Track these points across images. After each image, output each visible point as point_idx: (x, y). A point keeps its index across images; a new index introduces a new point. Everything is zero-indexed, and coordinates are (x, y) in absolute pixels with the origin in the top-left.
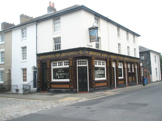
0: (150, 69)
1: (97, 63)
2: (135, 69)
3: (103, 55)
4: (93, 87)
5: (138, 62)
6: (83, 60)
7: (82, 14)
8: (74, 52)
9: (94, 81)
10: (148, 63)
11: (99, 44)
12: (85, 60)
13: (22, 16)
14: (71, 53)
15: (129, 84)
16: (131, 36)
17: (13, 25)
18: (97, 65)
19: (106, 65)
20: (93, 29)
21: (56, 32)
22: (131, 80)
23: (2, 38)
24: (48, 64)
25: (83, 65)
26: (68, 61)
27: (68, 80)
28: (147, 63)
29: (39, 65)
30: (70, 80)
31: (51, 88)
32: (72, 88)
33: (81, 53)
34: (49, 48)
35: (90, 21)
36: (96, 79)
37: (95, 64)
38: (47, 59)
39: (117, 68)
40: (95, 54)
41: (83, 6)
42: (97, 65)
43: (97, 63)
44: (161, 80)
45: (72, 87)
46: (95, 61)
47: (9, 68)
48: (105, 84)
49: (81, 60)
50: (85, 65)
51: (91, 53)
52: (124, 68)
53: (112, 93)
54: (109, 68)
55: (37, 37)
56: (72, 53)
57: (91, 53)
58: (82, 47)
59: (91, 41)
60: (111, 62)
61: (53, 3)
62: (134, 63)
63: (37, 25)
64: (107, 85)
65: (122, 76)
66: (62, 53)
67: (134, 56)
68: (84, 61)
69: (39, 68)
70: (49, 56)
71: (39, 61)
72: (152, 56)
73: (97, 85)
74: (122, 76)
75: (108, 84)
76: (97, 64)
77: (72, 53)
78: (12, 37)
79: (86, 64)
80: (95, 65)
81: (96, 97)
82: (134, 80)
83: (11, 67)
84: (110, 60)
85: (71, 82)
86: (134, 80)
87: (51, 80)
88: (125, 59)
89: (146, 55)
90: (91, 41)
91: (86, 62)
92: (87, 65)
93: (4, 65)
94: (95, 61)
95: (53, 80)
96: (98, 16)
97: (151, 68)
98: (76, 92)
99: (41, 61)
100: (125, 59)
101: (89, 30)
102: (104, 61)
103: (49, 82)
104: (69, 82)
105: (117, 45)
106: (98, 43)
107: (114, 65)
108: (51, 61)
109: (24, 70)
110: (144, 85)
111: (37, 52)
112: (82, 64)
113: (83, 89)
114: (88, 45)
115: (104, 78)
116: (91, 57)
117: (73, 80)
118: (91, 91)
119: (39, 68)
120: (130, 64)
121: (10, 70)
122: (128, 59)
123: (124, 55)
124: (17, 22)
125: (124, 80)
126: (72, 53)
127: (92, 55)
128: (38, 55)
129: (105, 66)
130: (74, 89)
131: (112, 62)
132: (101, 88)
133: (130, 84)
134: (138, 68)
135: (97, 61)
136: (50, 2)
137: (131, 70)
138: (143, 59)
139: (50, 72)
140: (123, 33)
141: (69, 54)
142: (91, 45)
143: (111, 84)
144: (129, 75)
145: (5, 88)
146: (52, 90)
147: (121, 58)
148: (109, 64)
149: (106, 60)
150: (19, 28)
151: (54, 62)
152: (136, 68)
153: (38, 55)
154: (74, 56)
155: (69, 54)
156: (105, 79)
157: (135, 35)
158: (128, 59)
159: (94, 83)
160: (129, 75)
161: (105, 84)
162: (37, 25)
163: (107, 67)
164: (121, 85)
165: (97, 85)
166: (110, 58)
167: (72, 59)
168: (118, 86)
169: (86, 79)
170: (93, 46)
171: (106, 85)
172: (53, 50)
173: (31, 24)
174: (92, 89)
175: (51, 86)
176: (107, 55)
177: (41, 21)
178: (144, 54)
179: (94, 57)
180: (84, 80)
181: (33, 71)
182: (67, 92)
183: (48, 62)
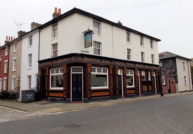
0: (176, 77)
1: (129, 72)
2: (152, 77)
4: (87, 96)
6: (78, 67)
7: (76, 17)
8: (67, 59)
9: (90, 90)
10: (173, 71)
12: (80, 67)
13: (33, 24)
14: (65, 60)
15: (143, 93)
16: (147, 41)
17: (24, 32)
18: (128, 74)
19: (134, 74)
20: (88, 33)
21: (55, 38)
22: (146, 90)
23: (16, 46)
24: (47, 71)
25: (78, 73)
26: (63, 68)
28: (173, 70)
29: (40, 72)
30: (64, 88)
31: (91, 97)
32: (65, 98)
33: (73, 59)
34: (47, 55)
35: (89, 24)
38: (47, 66)
39: (124, 76)
41: (75, 9)
42: (128, 74)
43: (129, 72)
44: (192, 89)
45: (65, 96)
46: (127, 71)
47: (19, 76)
48: (107, 93)
49: (76, 67)
50: (80, 73)
51: (86, 59)
52: (135, 76)
53: (101, 104)
54: (113, 75)
55: (39, 44)
56: (65, 59)
57: (86, 59)
58: (74, 53)
59: (86, 47)
60: (115, 69)
61: (60, 9)
62: (150, 71)
63: (40, 32)
66: (127, 62)
67: (151, 63)
68: (79, 68)
69: (40, 75)
70: (48, 63)
71: (40, 68)
72: (179, 63)
73: (94, 94)
75: (110, 93)
76: (128, 73)
77: (65, 59)
78: (22, 44)
79: (81, 71)
80: (127, 74)
81: (6, 106)
82: (150, 89)
83: (20, 74)
84: (115, 67)
85: (64, 90)
86: (150, 89)
89: (172, 61)
90: (86, 47)
91: (81, 69)
92: (82, 73)
93: (15, 73)
95: (51, 88)
96: (98, 20)
97: (177, 76)
98: (69, 102)
99: (42, 69)
100: (137, 65)
101: (85, 34)
102: (132, 71)
103: (47, 90)
104: (63, 91)
105: (126, 52)
106: (129, 54)
107: (120, 73)
108: (50, 68)
109: (30, 77)
110: (162, 95)
111: (39, 59)
112: (77, 71)
113: (77, 98)
114: (82, 51)
117: (66, 89)
118: (85, 101)
119: (40, 75)
121: (19, 77)
122: (141, 66)
123: (149, 63)
124: (28, 29)
125: (136, 89)
126: (66, 60)
128: (40, 62)
129: (107, 74)
130: (67, 98)
131: (118, 69)
132: (100, 98)
134: (157, 75)
135: (129, 71)
136: (56, 9)
137: (147, 78)
138: (161, 66)
139: (49, 79)
140: (135, 38)
141: (107, 62)
142: (87, 51)
143: (115, 93)
144: (143, 83)
145: (9, 95)
146: (49, 99)
147: (132, 65)
148: (113, 71)
149: (108, 67)
150: (27, 36)
151: (52, 70)
152: (154, 76)
153: (40, 62)
154: (67, 63)
155: (107, 62)
157: (152, 39)
158: (141, 66)
159: (89, 92)
160: (143, 83)
161: (107, 93)
162: (40, 32)
165: (94, 94)
166: (114, 65)
167: (66, 66)
168: (126, 96)
169: (81, 88)
170: (91, 51)
172: (52, 56)
174: (87, 99)
175: (48, 94)
176: (109, 62)
177: (44, 27)
178: (170, 60)
179: (91, 64)
180: (75, 89)
181: (36, 79)
182: (60, 101)
183: (47, 69)
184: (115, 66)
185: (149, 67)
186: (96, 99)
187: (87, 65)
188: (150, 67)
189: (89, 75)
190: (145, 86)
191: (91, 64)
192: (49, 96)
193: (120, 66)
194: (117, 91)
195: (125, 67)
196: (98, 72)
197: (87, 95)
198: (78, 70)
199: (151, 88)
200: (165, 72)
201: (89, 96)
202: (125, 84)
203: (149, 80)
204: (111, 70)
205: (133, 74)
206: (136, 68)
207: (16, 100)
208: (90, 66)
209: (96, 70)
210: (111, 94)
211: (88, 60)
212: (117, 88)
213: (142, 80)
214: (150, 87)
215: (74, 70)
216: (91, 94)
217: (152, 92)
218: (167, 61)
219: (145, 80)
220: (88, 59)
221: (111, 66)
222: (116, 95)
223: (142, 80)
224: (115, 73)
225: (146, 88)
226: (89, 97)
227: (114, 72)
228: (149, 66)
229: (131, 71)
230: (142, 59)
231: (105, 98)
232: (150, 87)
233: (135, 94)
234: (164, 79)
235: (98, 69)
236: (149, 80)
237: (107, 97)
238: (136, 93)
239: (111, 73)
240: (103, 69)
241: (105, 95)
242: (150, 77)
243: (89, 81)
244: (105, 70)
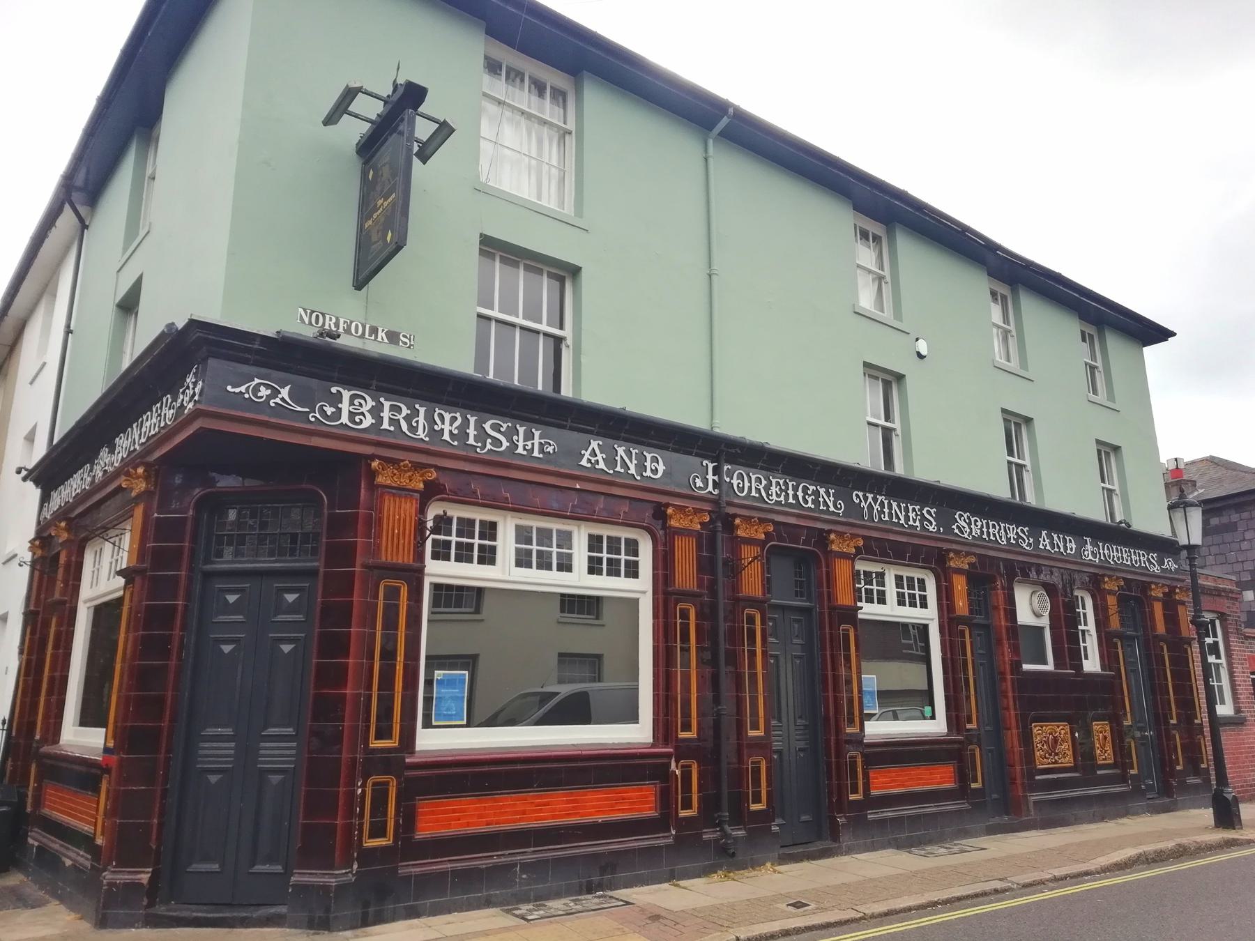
3: (1044, 542)
5: (1156, 569)
9: (858, 740)
11: (558, 341)
22: (1067, 760)
27: (260, 759)
31: (408, 847)
36: (878, 729)
37: (869, 592)
40: (1012, 535)
42: (882, 601)
64: (962, 791)
65: (633, 717)
73: (885, 783)
74: (633, 717)
75: (665, 799)
79: (633, 571)
80: (870, 600)
82: (1104, 753)
84: (728, 523)
86: (1104, 753)
87: (366, 741)
88: (968, 526)
91: (633, 548)
94: (861, 566)
100: (968, 526)
102: (916, 574)
106: (1016, 460)
115: (421, 727)
116: (822, 538)
120: (1050, 589)
127: (375, 438)
129: (929, 615)
132: (529, 855)
133: (303, 888)
137: (1069, 649)
148: (706, 565)
155: (641, 467)
156: (936, 726)
161: (940, 778)
163: (951, 620)
164: (887, 813)
171: (649, 812)
173: (144, 197)
178: (1246, 515)
179: (762, 521)
180: (228, 748)
184: (731, 510)
185: (1079, 552)
186: (468, 879)
187: (372, 474)
188: (1091, 552)
189: (393, 593)
190: (1048, 727)
191: (854, 536)
192: (1100, 765)
193: (792, 521)
194: (757, 771)
195: (1110, 577)
196: (901, 602)
197: (348, 829)
198: (605, 555)
199: (1109, 747)
200: (1225, 605)
201: (370, 843)
202: (851, 701)
203: (1092, 664)
204: (685, 554)
205: (635, 574)
206: (957, 553)
207: (115, 844)
208: (412, 485)
209: (506, 543)
210: (684, 813)
211: (994, 535)
212: (761, 746)
213: (1026, 667)
214: (1101, 729)
215: (623, 557)
216: (866, 775)
217: (1123, 779)
218: (1225, 520)
219: (1050, 667)
220: (994, 526)
221: (840, 535)
222: (740, 815)
223: (1026, 667)
224: (736, 587)
225: (1065, 747)
226: (368, 856)
227: (713, 572)
228: (1035, 535)
229: (910, 580)
230: (1016, 472)
231: (1100, 798)
232: (1101, 729)
233: (962, 805)
234: (1223, 661)
235: (523, 535)
236: (1092, 664)
237: (632, 843)
238: (962, 791)
239: (686, 576)
240: (899, 579)
241: (600, 819)
242: (1091, 645)
243: (389, 654)
244: (911, 587)
